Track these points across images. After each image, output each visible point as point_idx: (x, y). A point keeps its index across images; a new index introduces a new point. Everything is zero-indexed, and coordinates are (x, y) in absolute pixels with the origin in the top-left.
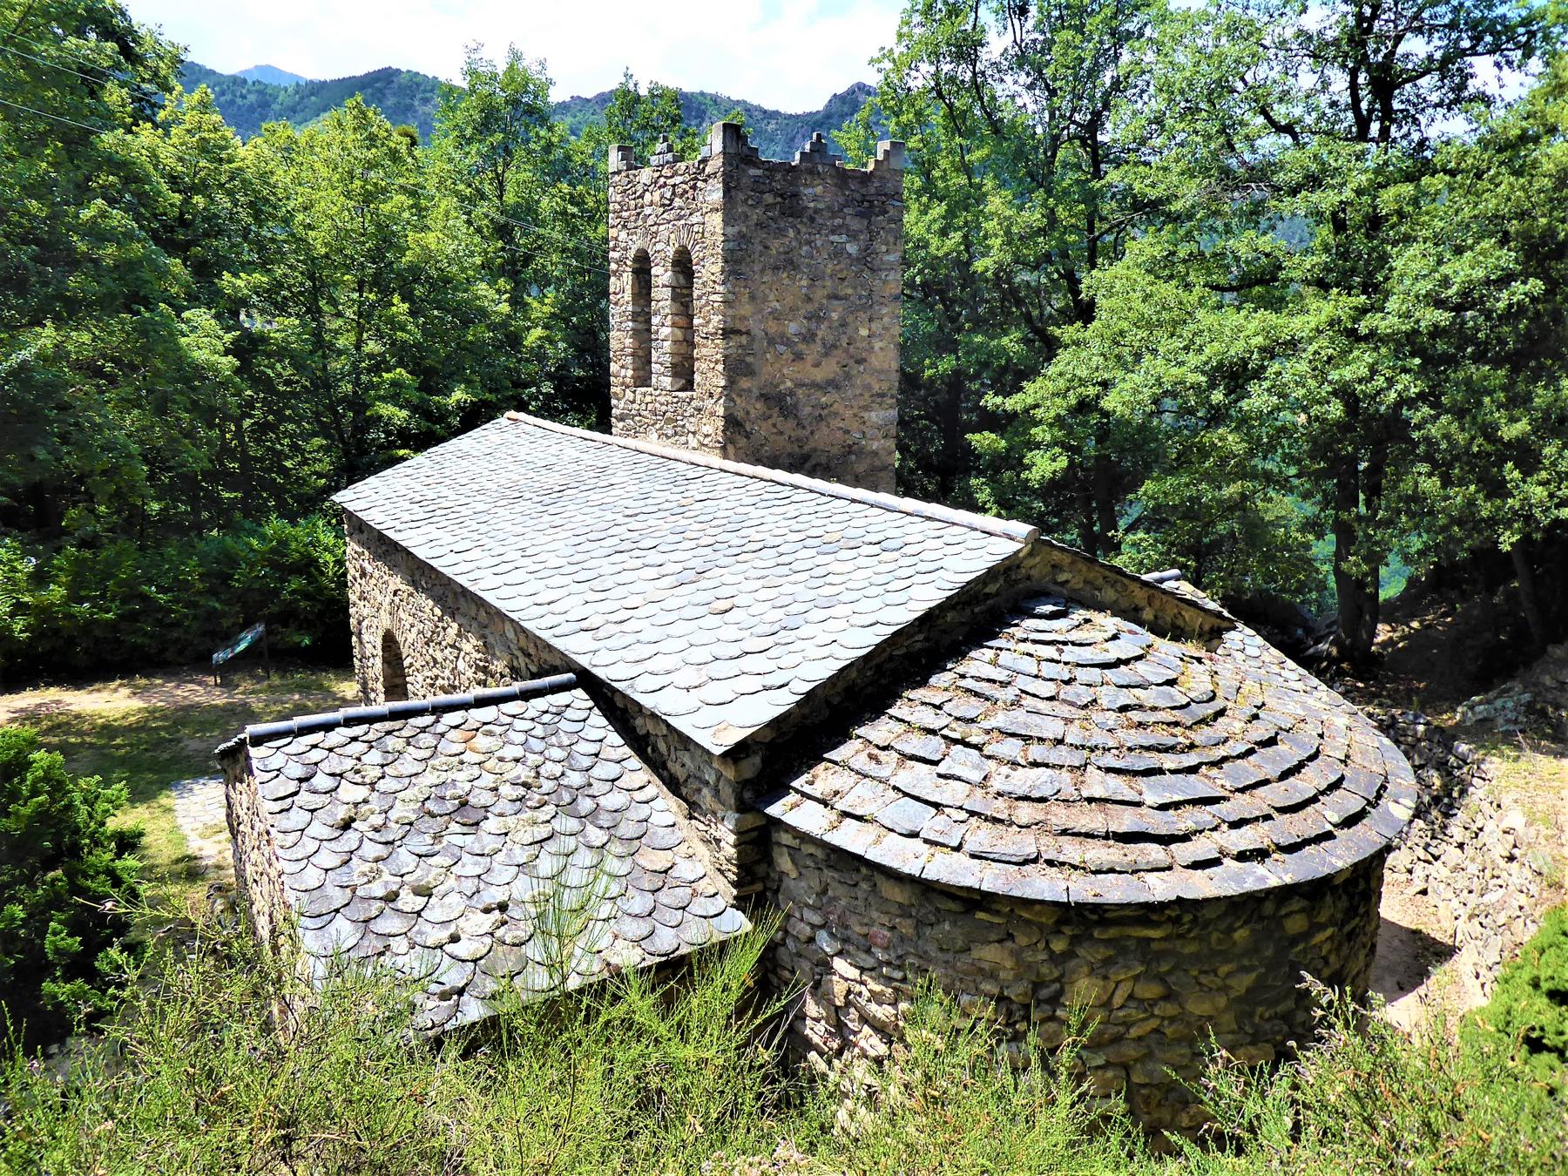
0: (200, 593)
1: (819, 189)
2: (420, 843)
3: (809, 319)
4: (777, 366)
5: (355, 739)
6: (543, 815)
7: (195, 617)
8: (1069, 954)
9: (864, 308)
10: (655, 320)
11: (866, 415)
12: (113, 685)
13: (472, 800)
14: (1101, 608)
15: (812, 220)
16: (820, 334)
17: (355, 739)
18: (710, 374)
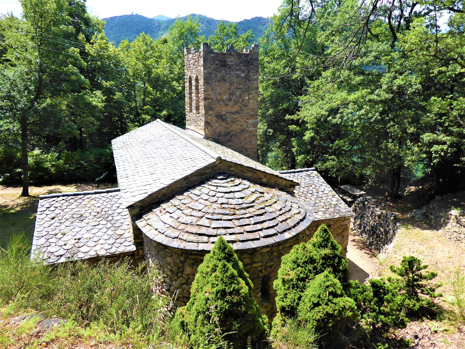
0: (94, 163)
1: (232, 59)
2: (67, 223)
3: (229, 95)
4: (220, 107)
5: (63, 200)
6: (99, 220)
7: (93, 169)
8: (185, 261)
9: (246, 91)
10: (193, 95)
11: (248, 121)
12: (72, 185)
13: (84, 215)
14: (244, 179)
15: (230, 67)
16: (233, 99)
17: (63, 200)
18: (202, 111)
